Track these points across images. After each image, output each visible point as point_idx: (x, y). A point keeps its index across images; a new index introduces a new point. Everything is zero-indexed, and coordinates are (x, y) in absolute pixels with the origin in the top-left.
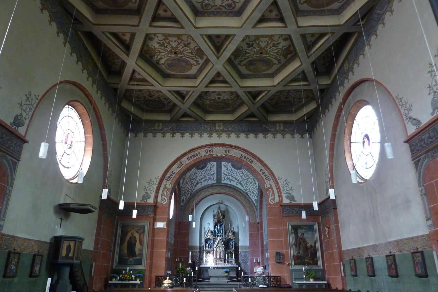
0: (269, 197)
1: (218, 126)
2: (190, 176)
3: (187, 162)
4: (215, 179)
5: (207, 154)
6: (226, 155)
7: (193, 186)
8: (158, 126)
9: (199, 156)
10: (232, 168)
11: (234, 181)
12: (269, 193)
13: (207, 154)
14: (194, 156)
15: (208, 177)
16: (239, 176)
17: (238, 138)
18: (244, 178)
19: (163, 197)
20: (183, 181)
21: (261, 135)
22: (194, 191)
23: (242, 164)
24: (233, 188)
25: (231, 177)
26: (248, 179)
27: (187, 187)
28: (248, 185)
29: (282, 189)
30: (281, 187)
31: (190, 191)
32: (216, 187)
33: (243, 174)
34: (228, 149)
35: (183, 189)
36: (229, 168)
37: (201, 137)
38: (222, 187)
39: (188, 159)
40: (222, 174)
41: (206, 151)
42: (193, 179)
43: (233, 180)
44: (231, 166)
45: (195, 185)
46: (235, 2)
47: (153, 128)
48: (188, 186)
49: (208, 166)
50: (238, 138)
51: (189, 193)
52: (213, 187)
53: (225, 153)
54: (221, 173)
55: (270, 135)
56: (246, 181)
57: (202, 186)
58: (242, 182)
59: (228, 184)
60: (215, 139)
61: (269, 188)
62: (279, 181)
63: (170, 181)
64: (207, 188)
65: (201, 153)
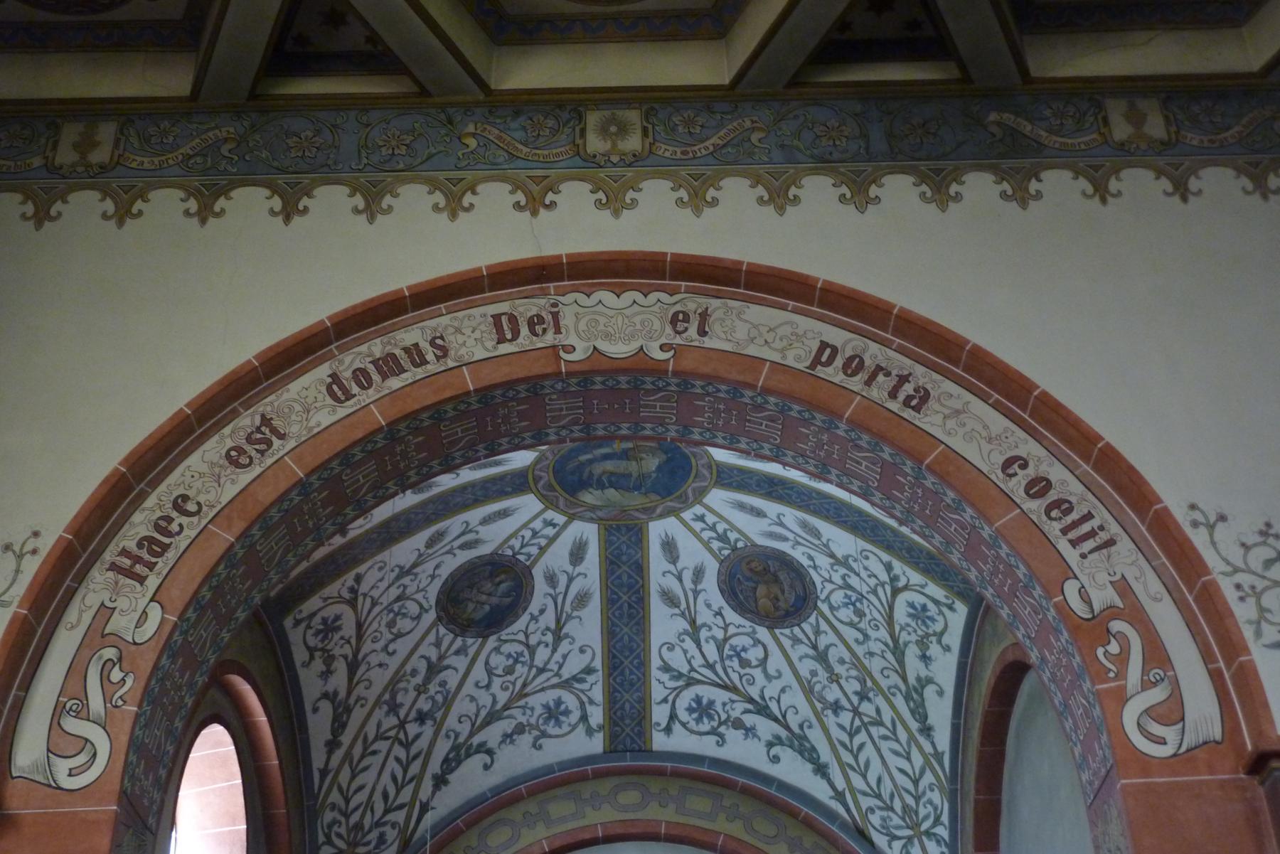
0: (1121, 698)
1: (603, 131)
2: (393, 685)
3: (324, 418)
4: (597, 716)
5: (505, 348)
6: (678, 350)
7: (419, 778)
8: (86, 144)
9: (432, 368)
10: (731, 616)
11: (750, 731)
12: (1122, 659)
13: (505, 348)
14: (388, 366)
15: (537, 701)
16: (788, 677)
17: (781, 210)
18: (833, 694)
19: (71, 724)
20: (339, 725)
21: (979, 188)
22: (429, 819)
23: (834, 415)
24: (746, 791)
25: (721, 696)
26: (863, 696)
27: (368, 778)
28: (869, 751)
29: (1243, 612)
30: (1230, 595)
31: (400, 816)
32: (606, 786)
33: (822, 657)
34: (692, 304)
35: (335, 797)
36: (704, 616)
37: (454, 207)
38: (655, 785)
39: (337, 389)
40: (655, 673)
41: (504, 328)
42: (421, 718)
43: (738, 724)
44: (718, 600)
45: (435, 766)
46: (676, 716)
47: (37, 162)
48: (377, 776)
49: (534, 607)
50: (781, 210)
51: (391, 834)
52: (587, 789)
53: (668, 336)
54: (643, 665)
55: (1058, 185)
56: (845, 718)
58: (815, 736)
59: (699, 759)
60: (576, 224)
61: (1111, 612)
62: (1199, 539)
63: (153, 582)
64: (533, 792)
65: (453, 340)
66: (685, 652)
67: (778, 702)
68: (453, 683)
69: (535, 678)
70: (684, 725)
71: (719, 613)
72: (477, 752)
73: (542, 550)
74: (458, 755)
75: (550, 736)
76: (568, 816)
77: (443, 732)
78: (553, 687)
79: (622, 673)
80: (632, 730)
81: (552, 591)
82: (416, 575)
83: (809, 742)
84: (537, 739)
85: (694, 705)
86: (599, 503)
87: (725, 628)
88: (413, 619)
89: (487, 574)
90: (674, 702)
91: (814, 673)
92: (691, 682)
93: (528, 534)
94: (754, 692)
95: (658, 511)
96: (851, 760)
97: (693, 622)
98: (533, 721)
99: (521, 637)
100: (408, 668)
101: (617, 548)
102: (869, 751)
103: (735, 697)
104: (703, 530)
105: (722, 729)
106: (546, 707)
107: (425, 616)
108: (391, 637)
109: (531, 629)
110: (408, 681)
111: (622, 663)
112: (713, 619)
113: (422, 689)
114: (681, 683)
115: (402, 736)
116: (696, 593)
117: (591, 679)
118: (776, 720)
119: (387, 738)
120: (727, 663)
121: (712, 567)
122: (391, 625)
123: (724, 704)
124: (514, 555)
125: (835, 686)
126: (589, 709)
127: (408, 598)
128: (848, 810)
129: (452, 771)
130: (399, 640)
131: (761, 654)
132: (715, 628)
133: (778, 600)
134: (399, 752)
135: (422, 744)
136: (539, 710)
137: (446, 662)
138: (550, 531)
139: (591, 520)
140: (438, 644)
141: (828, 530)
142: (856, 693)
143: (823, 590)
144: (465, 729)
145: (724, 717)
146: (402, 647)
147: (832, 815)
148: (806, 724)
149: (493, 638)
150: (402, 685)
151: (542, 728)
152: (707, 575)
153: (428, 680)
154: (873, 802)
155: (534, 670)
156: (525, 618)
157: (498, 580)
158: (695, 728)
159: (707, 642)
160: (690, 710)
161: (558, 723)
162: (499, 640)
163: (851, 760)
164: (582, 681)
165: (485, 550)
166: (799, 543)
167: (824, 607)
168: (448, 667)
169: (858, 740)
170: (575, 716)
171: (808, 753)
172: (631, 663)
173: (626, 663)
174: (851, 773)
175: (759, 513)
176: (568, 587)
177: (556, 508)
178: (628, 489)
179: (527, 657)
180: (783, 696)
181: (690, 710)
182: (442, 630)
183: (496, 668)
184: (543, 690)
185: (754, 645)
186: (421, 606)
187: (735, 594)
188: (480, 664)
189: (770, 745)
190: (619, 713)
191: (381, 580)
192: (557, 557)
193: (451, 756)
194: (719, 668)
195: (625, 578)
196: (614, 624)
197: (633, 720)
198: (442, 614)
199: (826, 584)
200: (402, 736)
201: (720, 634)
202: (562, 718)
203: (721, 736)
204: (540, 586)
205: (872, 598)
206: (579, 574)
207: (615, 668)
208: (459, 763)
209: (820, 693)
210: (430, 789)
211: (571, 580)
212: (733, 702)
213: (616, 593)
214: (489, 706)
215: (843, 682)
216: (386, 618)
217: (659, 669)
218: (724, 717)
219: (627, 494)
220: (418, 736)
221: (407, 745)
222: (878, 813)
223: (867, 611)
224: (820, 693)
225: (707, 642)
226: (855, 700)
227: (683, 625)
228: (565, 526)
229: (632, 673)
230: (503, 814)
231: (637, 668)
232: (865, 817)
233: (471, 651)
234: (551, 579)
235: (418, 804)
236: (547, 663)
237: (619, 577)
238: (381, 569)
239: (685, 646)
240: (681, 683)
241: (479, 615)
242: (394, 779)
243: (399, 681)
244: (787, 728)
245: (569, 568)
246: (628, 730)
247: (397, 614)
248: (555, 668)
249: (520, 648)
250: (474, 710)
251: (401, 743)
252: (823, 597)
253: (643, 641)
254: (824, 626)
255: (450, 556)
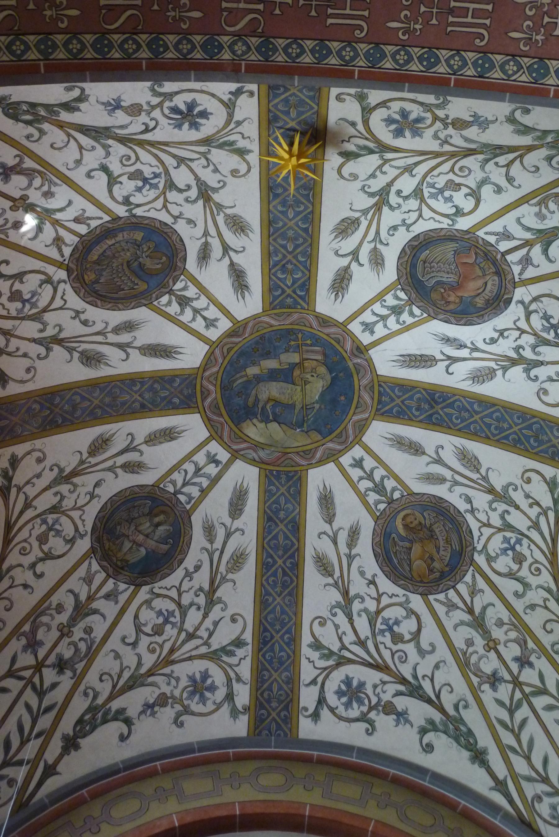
4: (243, 695)
7: (47, 735)
10: (385, 584)
11: (402, 717)
15: (184, 671)
18: (490, 664)
22: (52, 784)
24: (396, 781)
26: (524, 662)
32: (249, 767)
33: (478, 622)
36: (358, 586)
38: (300, 771)
40: (306, 651)
42: (61, 665)
43: (389, 709)
44: (372, 567)
45: (67, 725)
49: (189, 562)
52: (226, 770)
54: (294, 641)
56: (504, 691)
57: (128, 752)
58: (472, 718)
59: (348, 749)
66: (337, 627)
67: (432, 680)
68: (99, 633)
69: (184, 643)
70: (332, 710)
71: (372, 582)
72: (115, 719)
73: (204, 492)
74: (94, 718)
75: (193, 714)
76: (202, 796)
77: (82, 688)
78: (202, 657)
79: (272, 650)
80: (278, 714)
81: (209, 546)
82: (75, 486)
83: (465, 724)
84: (179, 715)
85: (343, 687)
86: (262, 440)
87: (378, 600)
88: (67, 541)
89: (147, 510)
90: (323, 684)
91: (470, 643)
92: (342, 662)
93: (190, 468)
94: (406, 671)
95: (318, 455)
96: (513, 742)
97: (345, 593)
98: (177, 693)
99: (174, 593)
100: (55, 600)
101: (275, 502)
102: (533, 726)
103: (387, 678)
104: (361, 478)
105: (372, 715)
106: (192, 678)
107: (79, 541)
108: (41, 555)
109: (184, 587)
110: (53, 618)
111: (272, 637)
112: (366, 590)
113: (66, 630)
114: (331, 662)
115: (36, 680)
116: (351, 558)
117: (240, 653)
118: (429, 701)
119: (20, 678)
120: (380, 638)
121: (368, 526)
122: (42, 539)
123: (375, 686)
124: (175, 494)
125: (492, 655)
126: (236, 686)
127: (64, 513)
128: (511, 802)
129: (84, 736)
130: (48, 562)
131: (414, 628)
132: (367, 598)
133: (432, 559)
134: (30, 697)
135: (57, 696)
136: (184, 682)
137: (95, 605)
138: (212, 470)
139: (253, 462)
140: (88, 580)
141: (489, 455)
142: (516, 659)
143: (480, 535)
144: (105, 689)
145: (374, 700)
146: (53, 570)
147: (495, 808)
148: (462, 703)
149: (145, 589)
150: (45, 619)
151: (186, 702)
152: (362, 536)
153: (73, 620)
154: (541, 788)
155: (183, 635)
156: (180, 573)
157: (157, 520)
158: (344, 714)
159: (359, 615)
160: (340, 693)
161: (203, 700)
162: (152, 592)
163: (513, 742)
164: (231, 654)
165: (147, 478)
166: (456, 483)
167: (480, 560)
168: (95, 612)
169: (519, 716)
170: (220, 694)
171: (464, 738)
172: (282, 637)
173: (277, 637)
174: (511, 756)
175: (416, 449)
176: (225, 543)
177: (220, 439)
178: (292, 426)
179: (178, 618)
180: (437, 673)
181: (340, 693)
182: (95, 566)
183: (145, 625)
184: (190, 658)
185: (407, 617)
186: (77, 529)
187: (390, 560)
188: (129, 617)
189: (423, 731)
190: (265, 695)
191: (38, 476)
192: (221, 496)
193: (87, 717)
194: (370, 645)
195: (281, 537)
196: (268, 594)
197: (280, 702)
198: (96, 545)
199: (484, 530)
200: (36, 680)
201: (372, 606)
202: (208, 694)
203: (371, 723)
204: (198, 538)
205: (534, 535)
206: (237, 530)
207: (265, 643)
208: (94, 729)
209: (477, 664)
210: (59, 751)
211: (228, 535)
212: (384, 683)
213: (272, 557)
214: (133, 667)
215: (501, 648)
216: (39, 529)
217: (310, 646)
218: (374, 700)
219: (290, 432)
220: (54, 686)
221: (41, 694)
222: (547, 800)
223: (527, 552)
224: (477, 664)
225: (359, 615)
226: (514, 667)
227: (336, 596)
228: (230, 463)
229: (282, 649)
230: (132, 787)
231: (288, 644)
232: (531, 807)
233: (123, 599)
234: (209, 531)
235: (42, 765)
236: (197, 629)
237: (275, 537)
238: (39, 461)
239: (337, 620)
240: (331, 662)
241: (133, 558)
242: (21, 728)
243: (43, 613)
244: (442, 710)
245: (227, 521)
246: (274, 714)
247: (50, 529)
248: (205, 635)
249: (172, 607)
250: (117, 669)
251: (34, 688)
252: (479, 547)
253: (295, 614)
254: (481, 583)
255: (111, 475)
